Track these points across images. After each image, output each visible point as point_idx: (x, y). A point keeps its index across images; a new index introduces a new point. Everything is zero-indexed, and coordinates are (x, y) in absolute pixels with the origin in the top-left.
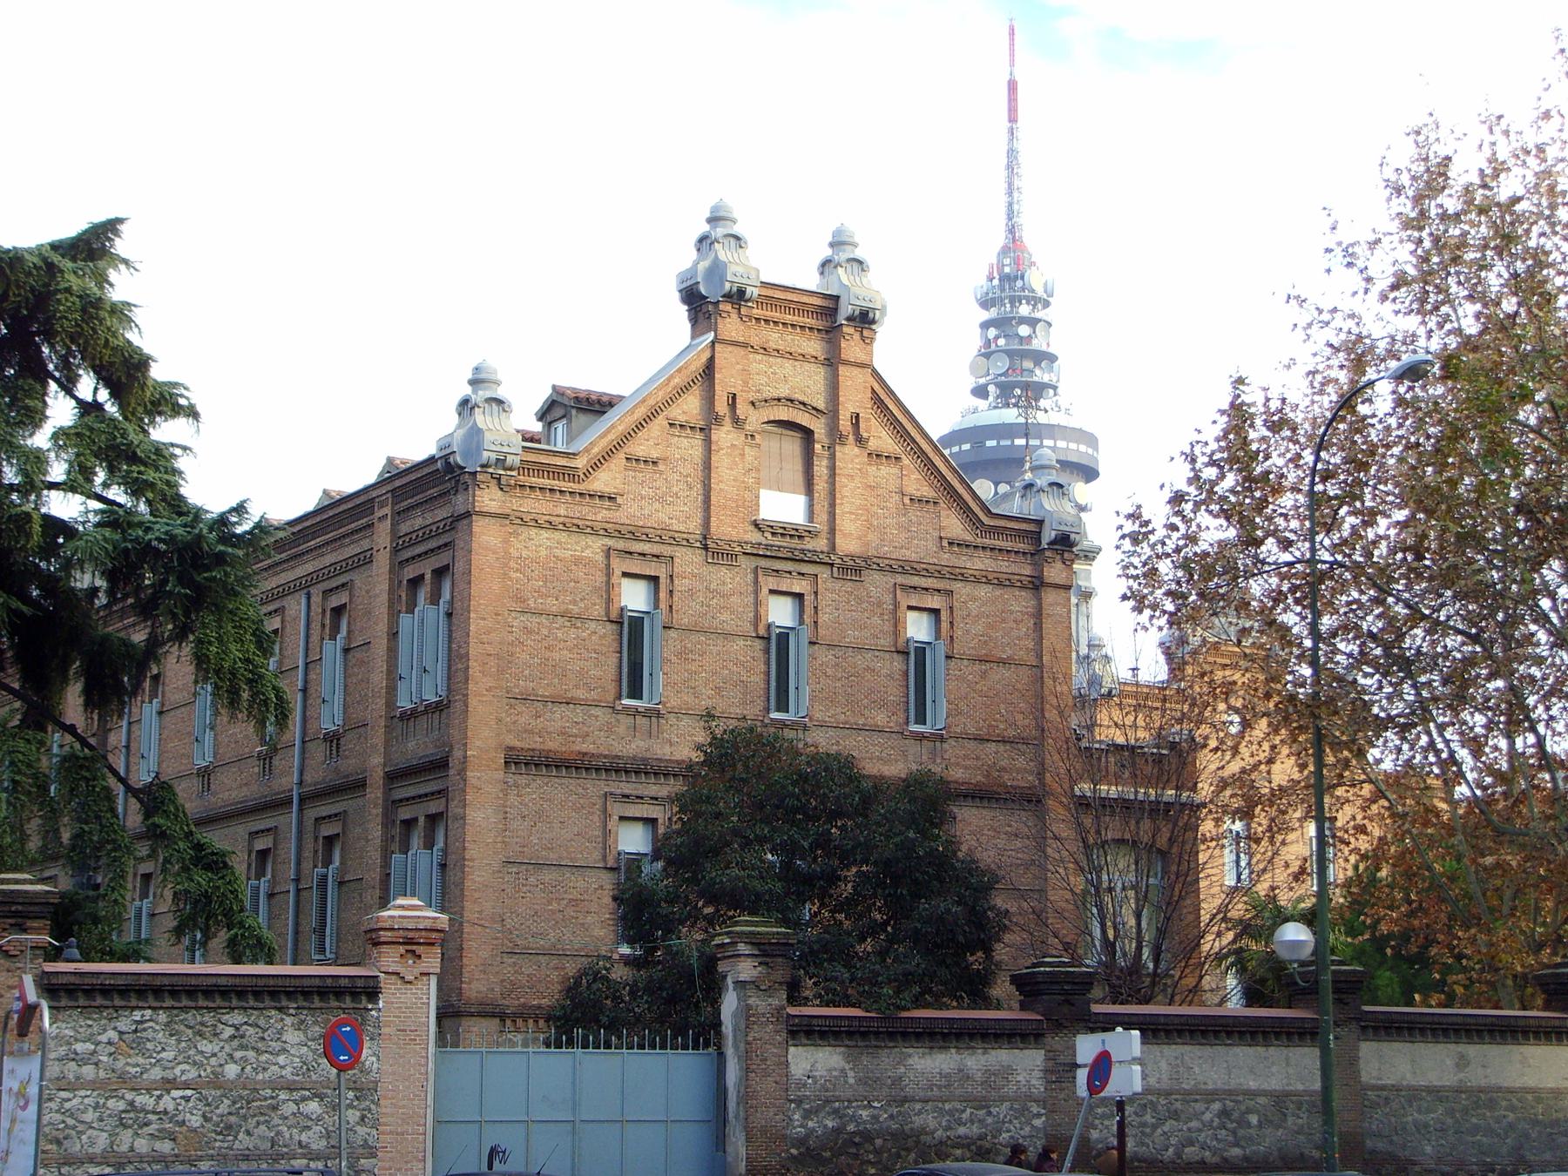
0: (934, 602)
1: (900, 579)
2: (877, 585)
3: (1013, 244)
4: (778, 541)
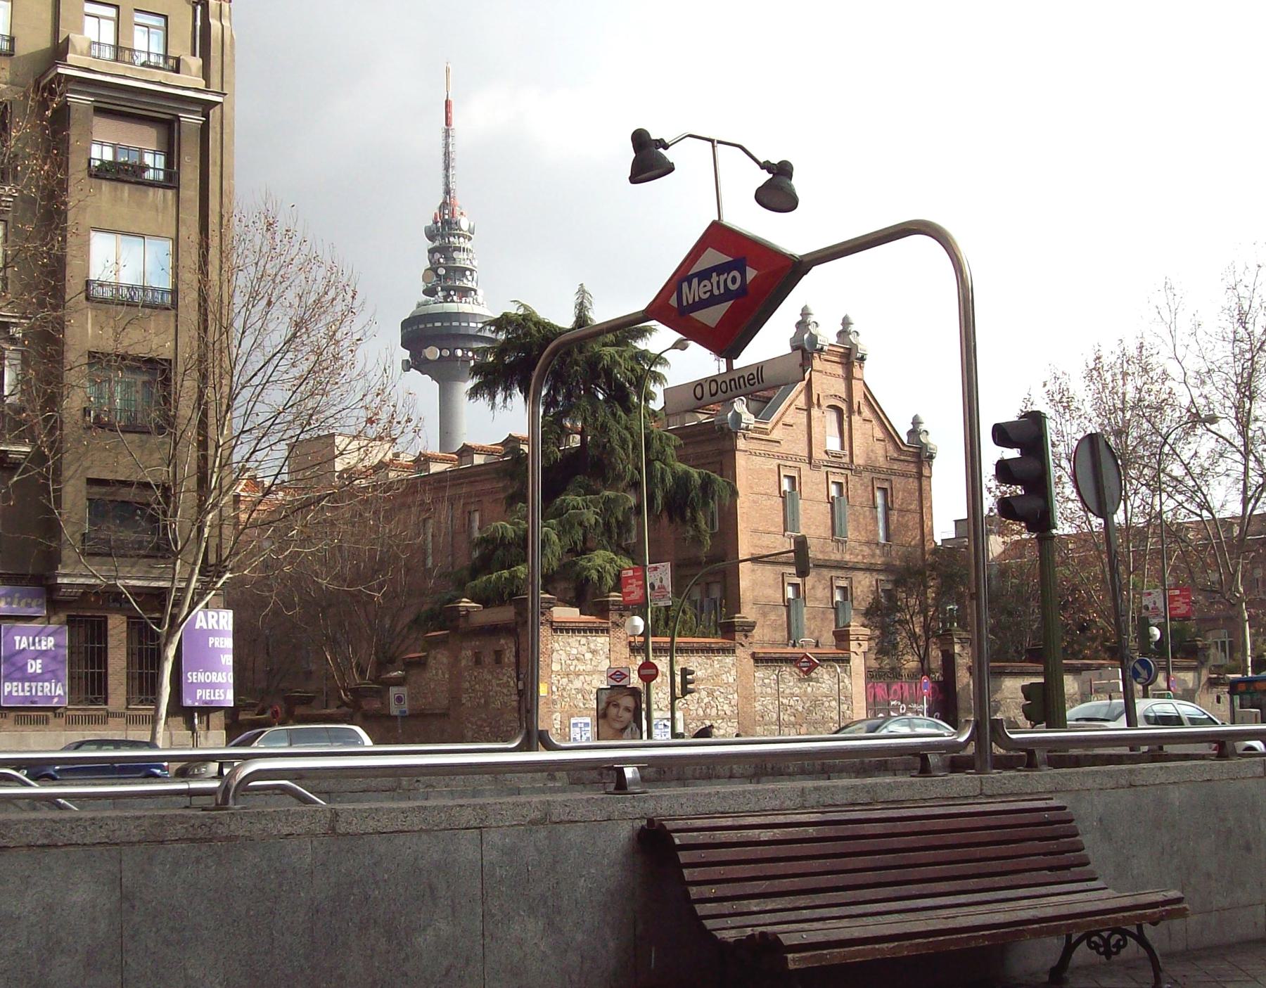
0: (886, 485)
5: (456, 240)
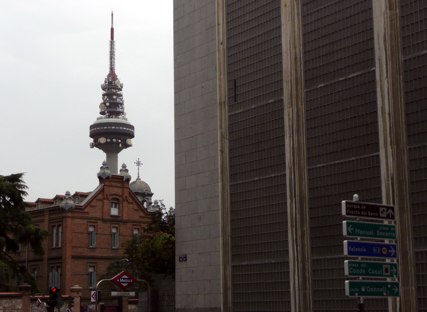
1: (133, 224)
2: (129, 225)
3: (112, 75)
4: (113, 218)
5: (115, 91)
